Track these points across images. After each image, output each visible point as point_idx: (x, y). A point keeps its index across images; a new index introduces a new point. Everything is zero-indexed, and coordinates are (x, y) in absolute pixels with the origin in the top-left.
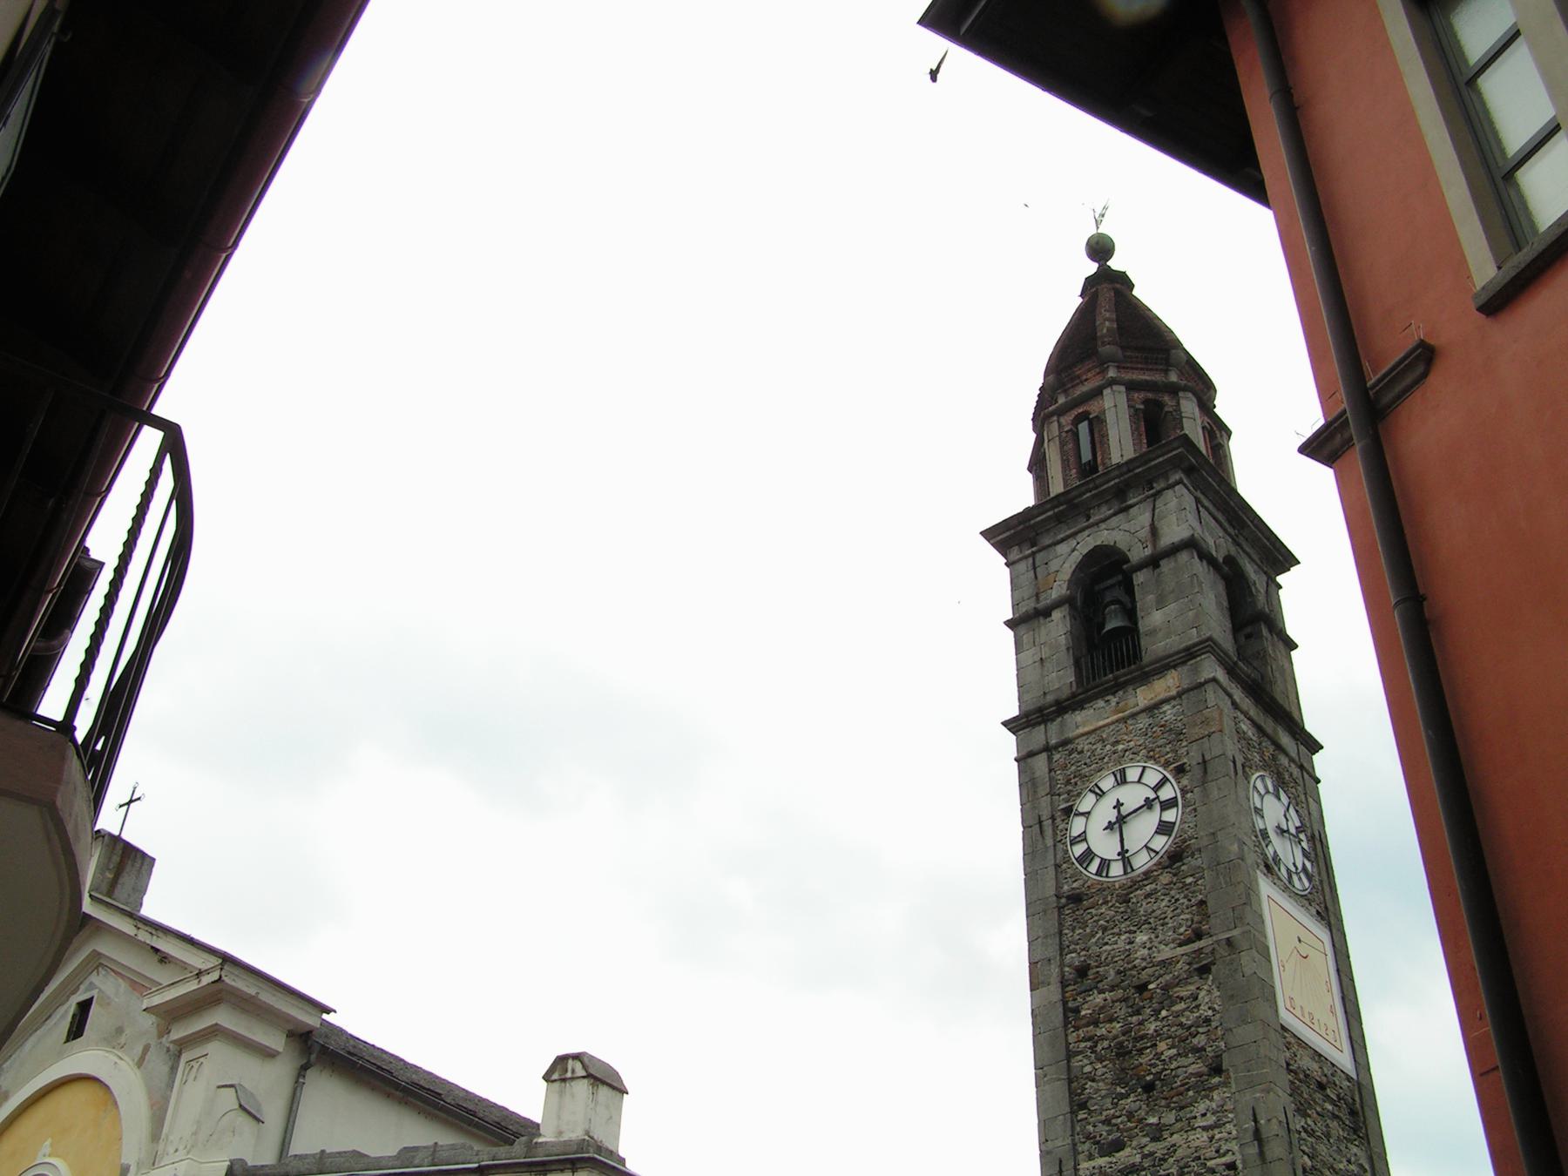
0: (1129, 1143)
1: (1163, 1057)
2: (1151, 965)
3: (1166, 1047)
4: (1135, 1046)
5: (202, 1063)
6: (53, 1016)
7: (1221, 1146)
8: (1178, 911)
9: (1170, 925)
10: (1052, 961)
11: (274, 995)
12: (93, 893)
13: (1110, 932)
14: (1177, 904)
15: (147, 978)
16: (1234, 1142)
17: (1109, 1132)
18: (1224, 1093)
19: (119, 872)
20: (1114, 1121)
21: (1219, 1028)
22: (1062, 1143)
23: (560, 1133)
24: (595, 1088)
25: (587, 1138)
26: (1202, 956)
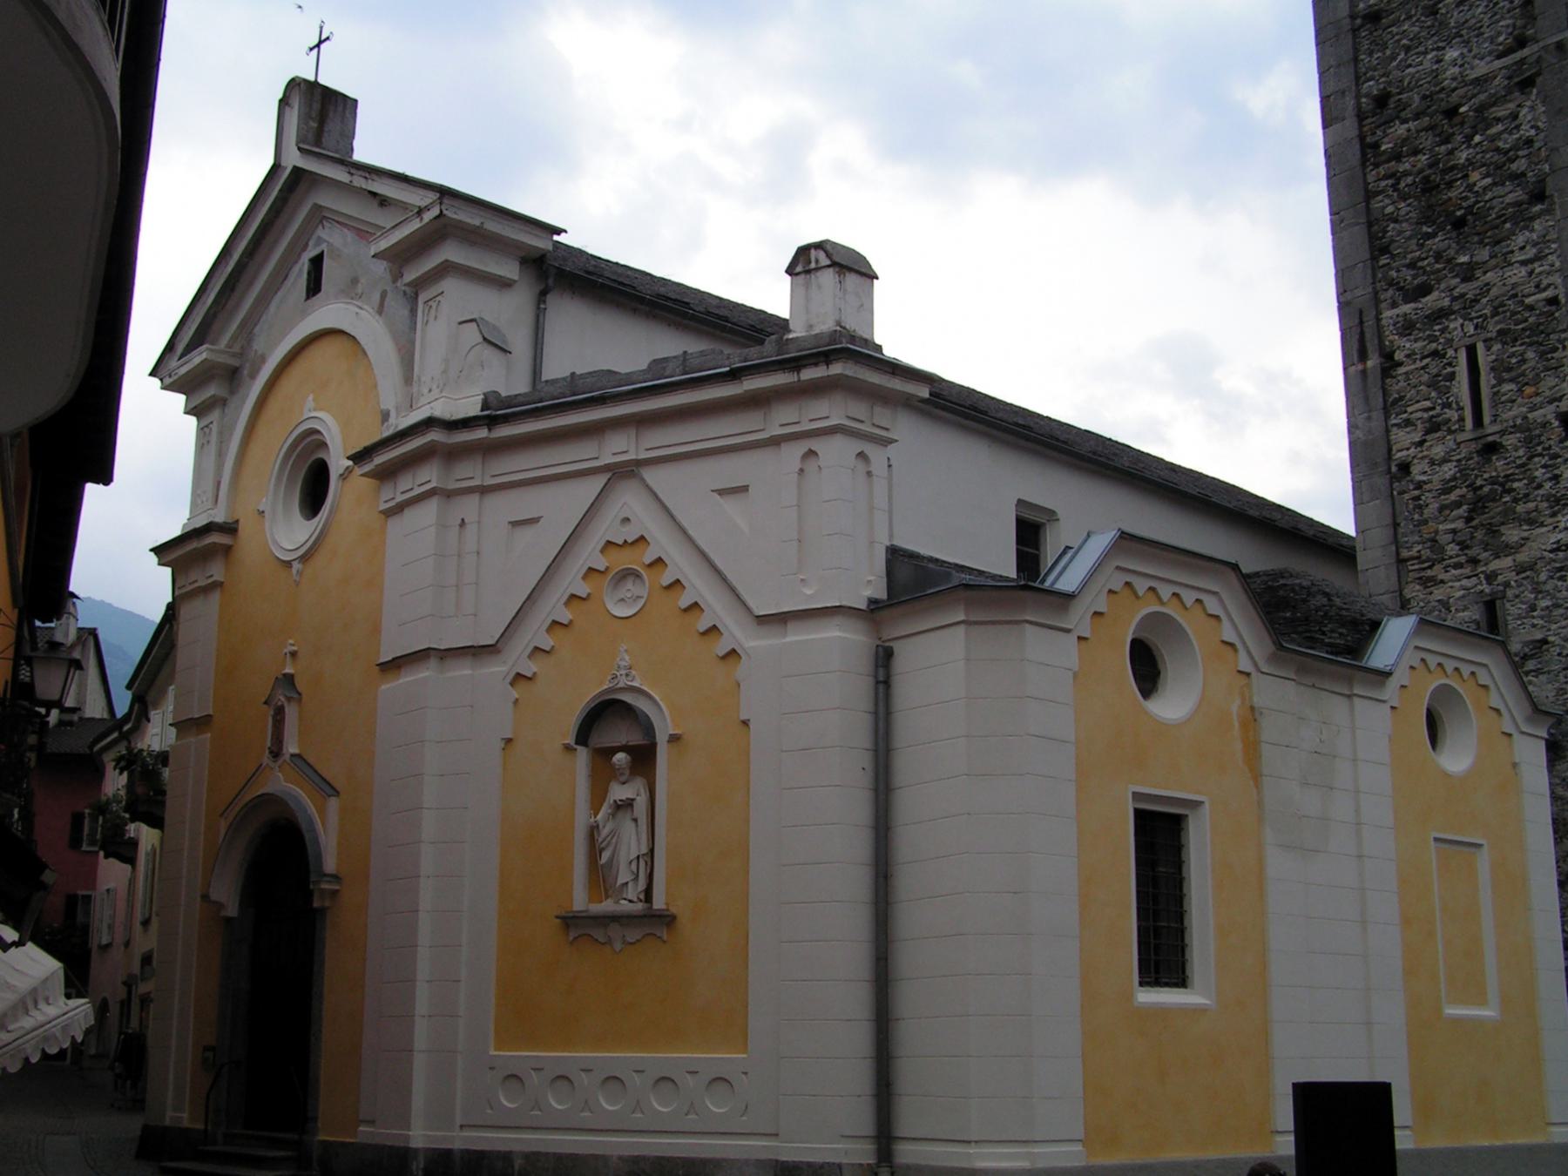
0: (1437, 286)
1: (1476, 189)
2: (1463, 84)
3: (1479, 177)
4: (1443, 179)
5: (439, 302)
6: (289, 276)
7: (1541, 280)
8: (1498, 17)
9: (1486, 35)
10: (1347, 93)
12: (302, 146)
13: (1413, 53)
14: (1495, 9)
15: (372, 224)
16: (1558, 274)
17: (1415, 277)
18: (1547, 221)
19: (322, 119)
20: (1420, 264)
21: (1543, 149)
22: (1362, 292)
23: (811, 327)
24: (842, 276)
25: (838, 328)
26: (1525, 67)
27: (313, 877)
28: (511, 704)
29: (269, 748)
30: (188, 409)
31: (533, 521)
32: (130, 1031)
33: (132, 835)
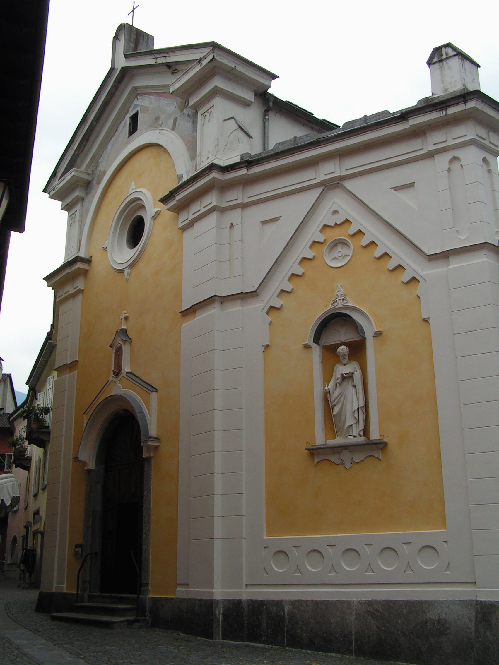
27: (143, 439)
28: (267, 325)
29: (113, 371)
31: (275, 220)
32: (28, 548)
33: (28, 456)
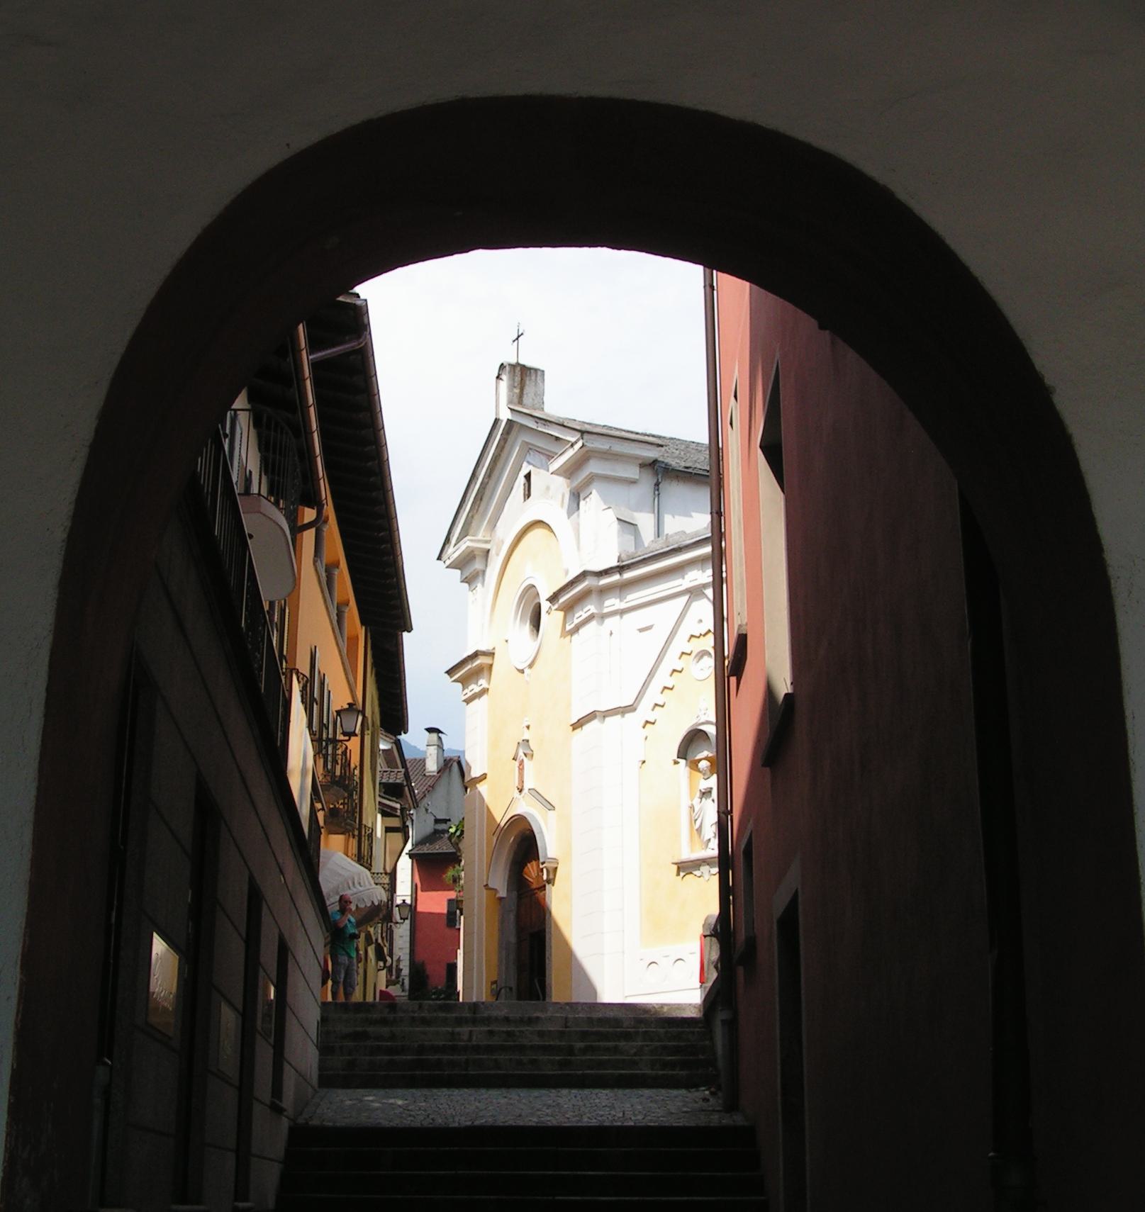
11: (622, 445)
12: (512, 407)
30: (462, 579)
